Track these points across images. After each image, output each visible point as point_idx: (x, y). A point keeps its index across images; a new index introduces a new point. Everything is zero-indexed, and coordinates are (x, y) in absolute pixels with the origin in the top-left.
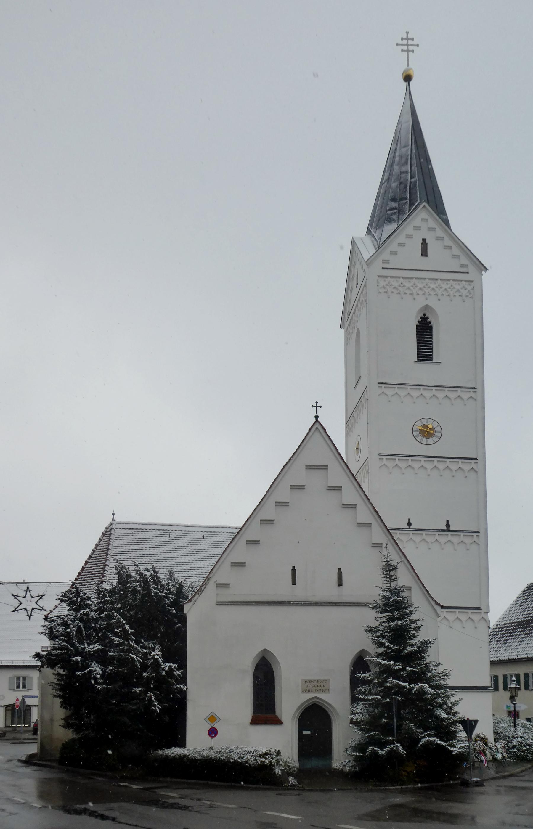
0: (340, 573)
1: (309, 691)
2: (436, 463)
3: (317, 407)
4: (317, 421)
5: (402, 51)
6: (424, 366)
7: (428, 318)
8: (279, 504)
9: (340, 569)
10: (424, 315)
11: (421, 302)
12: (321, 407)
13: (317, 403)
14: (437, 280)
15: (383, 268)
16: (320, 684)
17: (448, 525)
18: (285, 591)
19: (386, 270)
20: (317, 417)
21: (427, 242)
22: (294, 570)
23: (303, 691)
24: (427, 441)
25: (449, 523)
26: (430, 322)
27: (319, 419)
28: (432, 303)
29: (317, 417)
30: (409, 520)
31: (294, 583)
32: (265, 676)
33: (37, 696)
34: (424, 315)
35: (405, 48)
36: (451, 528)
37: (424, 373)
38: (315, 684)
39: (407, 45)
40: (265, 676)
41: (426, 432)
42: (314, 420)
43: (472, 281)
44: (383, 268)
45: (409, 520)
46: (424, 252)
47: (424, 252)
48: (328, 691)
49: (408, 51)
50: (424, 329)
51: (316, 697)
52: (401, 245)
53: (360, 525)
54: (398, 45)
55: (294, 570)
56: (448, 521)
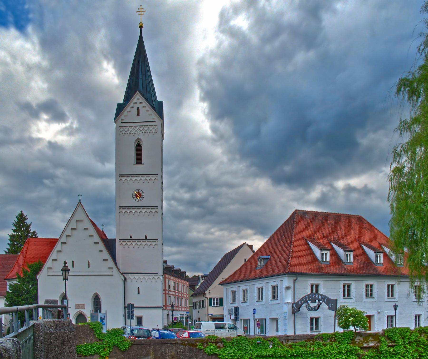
4: (80, 202)
6: (139, 166)
11: (137, 137)
20: (80, 200)
23: (76, 308)
28: (141, 137)
29: (80, 200)
48: (84, 308)
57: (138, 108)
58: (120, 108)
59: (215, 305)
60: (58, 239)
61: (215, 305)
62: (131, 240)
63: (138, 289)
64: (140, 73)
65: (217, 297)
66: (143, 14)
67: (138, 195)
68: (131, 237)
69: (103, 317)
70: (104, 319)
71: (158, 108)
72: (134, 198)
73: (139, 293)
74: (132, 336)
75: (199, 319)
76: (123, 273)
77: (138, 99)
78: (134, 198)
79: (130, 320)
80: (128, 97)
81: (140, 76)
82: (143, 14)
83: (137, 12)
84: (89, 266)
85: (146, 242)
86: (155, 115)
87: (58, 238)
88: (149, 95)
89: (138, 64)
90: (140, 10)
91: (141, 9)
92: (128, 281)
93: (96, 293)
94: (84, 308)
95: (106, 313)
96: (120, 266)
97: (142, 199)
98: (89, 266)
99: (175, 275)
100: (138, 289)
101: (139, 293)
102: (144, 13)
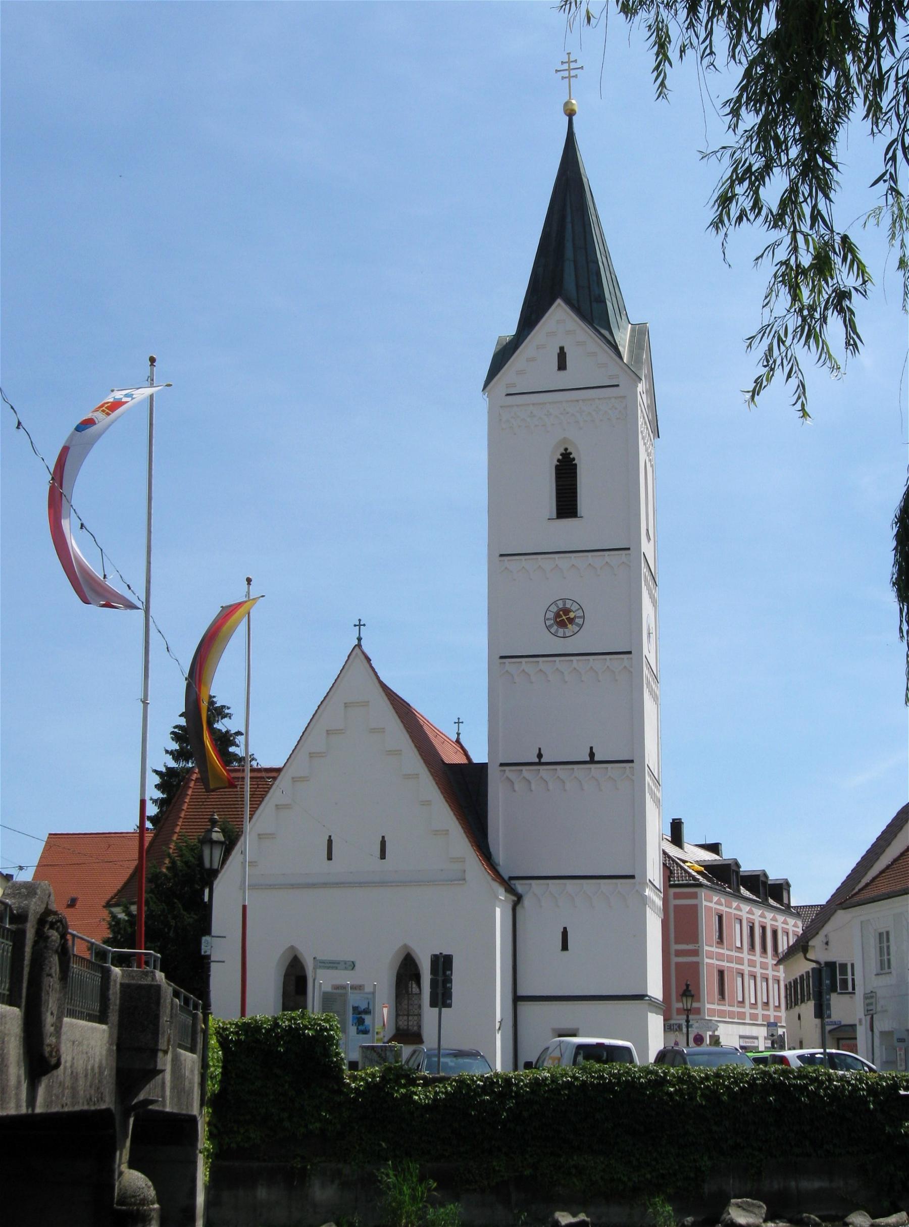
2: (575, 664)
4: (359, 645)
6: (567, 523)
7: (571, 453)
8: (312, 755)
10: (566, 449)
14: (577, 401)
17: (592, 754)
18: (318, 865)
19: (510, 397)
20: (359, 639)
24: (564, 633)
25: (594, 751)
27: (362, 642)
29: (359, 639)
30: (540, 749)
31: (330, 858)
33: (243, 1014)
34: (566, 449)
35: (566, 74)
36: (596, 759)
37: (568, 532)
41: (563, 618)
42: (356, 642)
43: (624, 397)
45: (540, 749)
50: (566, 471)
52: (531, 360)
53: (407, 777)
56: (591, 748)
57: (562, 349)
58: (504, 354)
60: (278, 770)
62: (540, 763)
63: (565, 933)
64: (569, 245)
66: (576, 76)
67: (563, 618)
68: (540, 756)
69: (363, 1006)
70: (367, 1011)
72: (551, 626)
73: (565, 947)
75: (801, 1043)
76: (511, 878)
77: (560, 319)
78: (551, 626)
79: (436, 1010)
80: (531, 316)
81: (569, 253)
82: (576, 76)
83: (557, 71)
84: (383, 856)
85: (593, 766)
87: (279, 764)
89: (563, 218)
90: (566, 66)
92: (527, 902)
93: (405, 946)
95: (373, 993)
96: (500, 855)
97: (548, 623)
98: (383, 856)
99: (743, 890)
100: (565, 933)
101: (565, 947)
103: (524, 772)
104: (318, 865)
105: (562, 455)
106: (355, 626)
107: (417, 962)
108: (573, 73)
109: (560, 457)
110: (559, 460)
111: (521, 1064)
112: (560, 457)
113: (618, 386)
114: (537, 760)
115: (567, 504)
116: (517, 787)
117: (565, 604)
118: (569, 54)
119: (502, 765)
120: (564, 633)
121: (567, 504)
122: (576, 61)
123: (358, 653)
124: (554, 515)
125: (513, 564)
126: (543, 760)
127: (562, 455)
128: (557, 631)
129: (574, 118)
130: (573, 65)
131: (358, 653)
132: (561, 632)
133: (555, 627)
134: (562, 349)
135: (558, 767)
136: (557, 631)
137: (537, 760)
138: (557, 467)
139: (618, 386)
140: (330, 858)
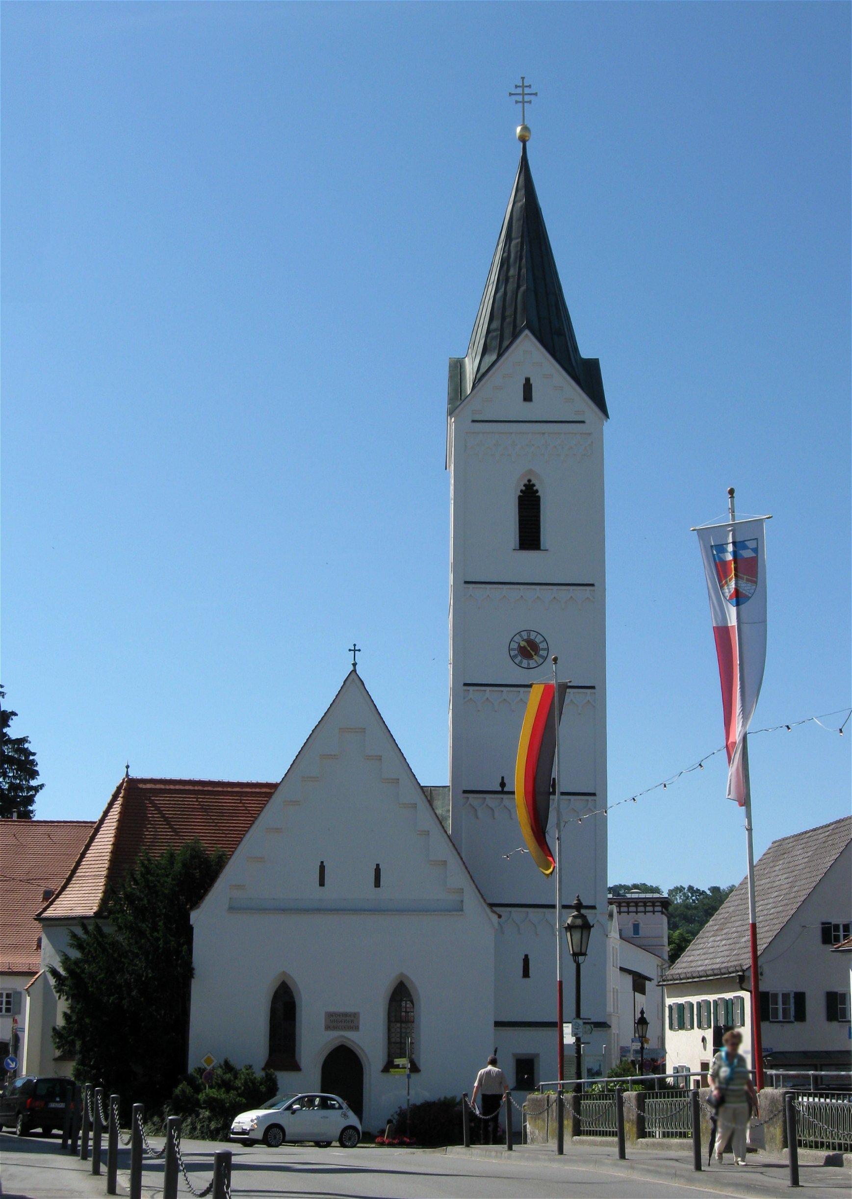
0: (378, 871)
1: (335, 1028)
3: (355, 650)
4: (354, 671)
5: (517, 102)
9: (378, 865)
10: (529, 481)
12: (359, 650)
13: (355, 645)
14: (544, 434)
15: (473, 421)
16: (348, 1018)
18: (312, 892)
20: (355, 665)
21: (531, 382)
22: (322, 868)
23: (327, 1028)
24: (529, 664)
25: (505, 781)
26: (537, 491)
29: (355, 665)
30: (503, 778)
31: (322, 883)
32: (284, 1006)
34: (529, 481)
35: (520, 98)
37: (529, 563)
38: (791, 840)
39: (523, 94)
40: (284, 1006)
41: (528, 649)
42: (352, 668)
43: (590, 434)
44: (473, 421)
45: (503, 778)
46: (528, 396)
47: (528, 396)
48: (356, 1028)
49: (523, 102)
50: (529, 503)
51: (343, 1036)
54: (511, 94)
55: (322, 868)
57: (528, 380)
59: (781, 1018)
61: (781, 1018)
62: (502, 792)
63: (526, 960)
65: (785, 991)
66: (530, 102)
68: (503, 784)
71: (588, 377)
72: (515, 656)
73: (526, 974)
74: (230, 1080)
78: (515, 656)
82: (530, 102)
84: (377, 884)
86: (576, 399)
88: (556, 336)
90: (519, 91)
91: (523, 87)
94: (356, 1028)
97: (512, 653)
98: (377, 884)
100: (526, 960)
101: (526, 974)
102: (532, 98)
103: (487, 800)
104: (366, 891)
105: (525, 485)
106: (350, 650)
107: (295, 994)
108: (527, 98)
109: (524, 488)
110: (522, 491)
111: (584, 1072)
112: (524, 488)
113: (583, 422)
114: (500, 789)
115: (530, 536)
116: (480, 814)
117: (529, 636)
118: (523, 78)
119: (465, 792)
120: (529, 664)
121: (530, 536)
122: (530, 86)
123: (353, 681)
124: (518, 547)
125: (479, 591)
126: (506, 789)
127: (525, 485)
128: (521, 662)
129: (528, 144)
130: (527, 91)
131: (353, 681)
132: (525, 663)
133: (519, 658)
134: (528, 380)
135: (487, 796)
136: (521, 662)
137: (500, 789)
138: (520, 497)
139: (583, 422)
140: (322, 883)
